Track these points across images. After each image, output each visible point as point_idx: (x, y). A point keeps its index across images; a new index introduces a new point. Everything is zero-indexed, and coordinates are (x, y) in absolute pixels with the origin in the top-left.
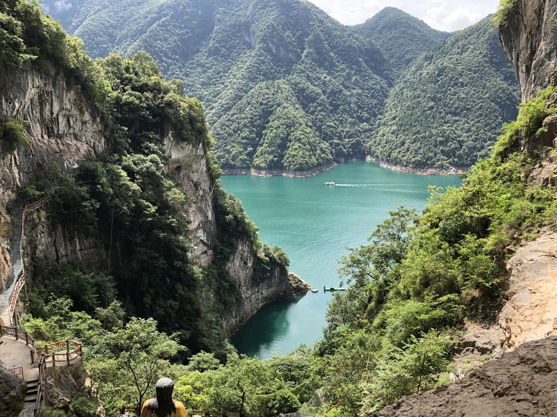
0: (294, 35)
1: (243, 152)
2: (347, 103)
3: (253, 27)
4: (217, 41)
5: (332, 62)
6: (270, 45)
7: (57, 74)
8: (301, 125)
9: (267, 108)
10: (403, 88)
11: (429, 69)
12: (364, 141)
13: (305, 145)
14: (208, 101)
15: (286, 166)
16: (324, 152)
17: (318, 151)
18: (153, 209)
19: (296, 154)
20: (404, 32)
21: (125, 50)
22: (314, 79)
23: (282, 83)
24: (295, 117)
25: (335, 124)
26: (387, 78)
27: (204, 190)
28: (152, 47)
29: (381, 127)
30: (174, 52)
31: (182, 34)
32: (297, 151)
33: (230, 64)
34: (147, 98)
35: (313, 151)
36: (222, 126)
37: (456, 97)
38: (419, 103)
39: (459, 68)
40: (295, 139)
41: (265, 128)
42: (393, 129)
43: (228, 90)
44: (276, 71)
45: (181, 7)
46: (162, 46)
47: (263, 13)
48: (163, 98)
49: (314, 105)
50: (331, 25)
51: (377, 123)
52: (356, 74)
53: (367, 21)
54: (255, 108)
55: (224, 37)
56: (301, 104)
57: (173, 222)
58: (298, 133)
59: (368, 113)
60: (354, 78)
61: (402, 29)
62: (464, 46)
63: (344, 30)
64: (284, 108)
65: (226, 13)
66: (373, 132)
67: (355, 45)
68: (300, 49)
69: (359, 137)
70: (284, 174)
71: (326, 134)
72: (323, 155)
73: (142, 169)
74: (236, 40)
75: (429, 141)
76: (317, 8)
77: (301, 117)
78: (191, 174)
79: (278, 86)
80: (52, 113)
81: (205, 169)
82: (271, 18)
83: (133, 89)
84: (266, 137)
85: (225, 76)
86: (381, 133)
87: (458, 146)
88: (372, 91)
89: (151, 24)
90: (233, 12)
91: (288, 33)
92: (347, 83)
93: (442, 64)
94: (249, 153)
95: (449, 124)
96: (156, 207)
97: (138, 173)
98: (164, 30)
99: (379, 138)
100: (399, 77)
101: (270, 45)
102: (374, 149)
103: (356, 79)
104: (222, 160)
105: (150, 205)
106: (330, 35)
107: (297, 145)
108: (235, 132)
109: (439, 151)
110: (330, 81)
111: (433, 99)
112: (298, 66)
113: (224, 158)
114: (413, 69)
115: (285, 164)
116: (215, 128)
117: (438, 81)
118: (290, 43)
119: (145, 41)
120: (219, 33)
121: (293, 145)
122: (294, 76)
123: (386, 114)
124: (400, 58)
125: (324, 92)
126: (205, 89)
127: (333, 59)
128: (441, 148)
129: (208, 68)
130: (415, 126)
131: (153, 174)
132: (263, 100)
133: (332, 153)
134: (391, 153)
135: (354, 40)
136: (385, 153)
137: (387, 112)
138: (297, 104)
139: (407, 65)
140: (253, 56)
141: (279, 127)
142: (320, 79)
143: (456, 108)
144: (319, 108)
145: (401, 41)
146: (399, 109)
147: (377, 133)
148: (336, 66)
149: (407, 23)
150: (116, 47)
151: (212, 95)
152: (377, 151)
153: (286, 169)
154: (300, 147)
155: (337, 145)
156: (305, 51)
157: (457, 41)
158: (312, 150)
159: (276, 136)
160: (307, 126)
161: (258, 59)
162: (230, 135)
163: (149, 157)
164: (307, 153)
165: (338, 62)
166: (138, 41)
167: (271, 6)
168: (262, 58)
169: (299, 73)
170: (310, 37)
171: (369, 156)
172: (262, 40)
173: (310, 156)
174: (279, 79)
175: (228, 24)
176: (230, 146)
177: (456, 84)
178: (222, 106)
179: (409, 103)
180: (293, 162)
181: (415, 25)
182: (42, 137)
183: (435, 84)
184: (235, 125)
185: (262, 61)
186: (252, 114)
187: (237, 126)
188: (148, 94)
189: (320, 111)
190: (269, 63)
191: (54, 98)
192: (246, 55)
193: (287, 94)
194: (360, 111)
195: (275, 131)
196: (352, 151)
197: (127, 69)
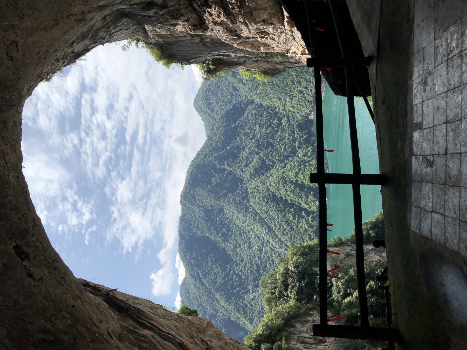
0: (215, 176)
1: (305, 219)
3: (208, 207)
4: (217, 234)
5: (234, 148)
6: (221, 194)
7: (287, 331)
8: (284, 172)
9: (271, 198)
10: (256, 93)
12: (297, 121)
14: (262, 244)
16: (306, 154)
18: (372, 283)
20: (213, 93)
21: (222, 307)
23: (251, 185)
24: (278, 176)
25: (283, 145)
26: (247, 105)
27: (351, 250)
28: (221, 286)
30: (225, 268)
31: (212, 261)
33: (234, 226)
34: (292, 282)
35: (306, 163)
36: (284, 234)
41: (286, 201)
42: (289, 100)
43: (254, 228)
44: (241, 190)
45: (192, 260)
46: (220, 277)
47: (198, 198)
48: (292, 272)
49: (267, 161)
51: (282, 112)
52: (244, 129)
53: (203, 120)
54: (270, 207)
55: (214, 229)
56: (267, 171)
57: (380, 271)
58: (291, 175)
59: (274, 119)
60: (247, 130)
61: (211, 94)
63: (211, 139)
64: (270, 185)
65: (197, 227)
66: (290, 114)
67: (223, 131)
68: (224, 171)
69: (293, 126)
71: (291, 152)
72: (309, 155)
73: (343, 288)
74: (217, 220)
75: (300, 72)
76: (195, 158)
78: (340, 258)
80: (310, 338)
81: (335, 248)
82: (202, 193)
83: (286, 290)
84: (294, 200)
85: (243, 229)
86: (291, 109)
88: (257, 116)
89: (203, 285)
90: (196, 221)
91: (213, 180)
94: (306, 214)
96: (371, 281)
97: (346, 291)
98: (209, 275)
99: (295, 110)
100: (246, 96)
101: (221, 194)
103: (248, 129)
104: (313, 237)
105: (369, 284)
106: (214, 149)
107: (300, 175)
108: (289, 224)
110: (249, 149)
112: (238, 173)
113: (310, 235)
114: (241, 85)
116: (286, 240)
118: (221, 179)
119: (217, 290)
120: (211, 233)
121: (301, 178)
122: (245, 177)
123: (276, 104)
124: (232, 95)
125: (258, 153)
126: (253, 247)
127: (232, 147)
129: (237, 243)
130: (287, 83)
131: (346, 281)
132: (264, 201)
133: (307, 147)
134: (308, 101)
135: (219, 131)
137: (274, 105)
138: (267, 174)
139: (237, 90)
140: (229, 207)
141: (286, 189)
142: (247, 157)
144: (270, 157)
145: (219, 95)
146: (273, 96)
147: (291, 111)
148: (238, 144)
149: (206, 91)
150: (219, 313)
151: (258, 241)
152: (306, 111)
154: (302, 173)
155: (300, 143)
156: (226, 168)
159: (293, 193)
160: (284, 167)
161: (232, 204)
162: (291, 228)
163: (334, 283)
164: (308, 167)
165: (235, 143)
166: (216, 296)
167: (194, 192)
168: (231, 200)
170: (216, 164)
171: (310, 117)
172: (218, 200)
173: (309, 165)
174: (247, 189)
175: (205, 225)
176: (301, 229)
178: (267, 233)
179: (269, 89)
181: (207, 85)
182: (326, 345)
184: (284, 224)
185: (233, 200)
186: (275, 210)
187: (284, 223)
188: (290, 281)
189: (272, 157)
190: (235, 195)
191: (301, 336)
192: (228, 212)
194: (273, 125)
195: (289, 193)
196: (305, 130)
197: (273, 293)
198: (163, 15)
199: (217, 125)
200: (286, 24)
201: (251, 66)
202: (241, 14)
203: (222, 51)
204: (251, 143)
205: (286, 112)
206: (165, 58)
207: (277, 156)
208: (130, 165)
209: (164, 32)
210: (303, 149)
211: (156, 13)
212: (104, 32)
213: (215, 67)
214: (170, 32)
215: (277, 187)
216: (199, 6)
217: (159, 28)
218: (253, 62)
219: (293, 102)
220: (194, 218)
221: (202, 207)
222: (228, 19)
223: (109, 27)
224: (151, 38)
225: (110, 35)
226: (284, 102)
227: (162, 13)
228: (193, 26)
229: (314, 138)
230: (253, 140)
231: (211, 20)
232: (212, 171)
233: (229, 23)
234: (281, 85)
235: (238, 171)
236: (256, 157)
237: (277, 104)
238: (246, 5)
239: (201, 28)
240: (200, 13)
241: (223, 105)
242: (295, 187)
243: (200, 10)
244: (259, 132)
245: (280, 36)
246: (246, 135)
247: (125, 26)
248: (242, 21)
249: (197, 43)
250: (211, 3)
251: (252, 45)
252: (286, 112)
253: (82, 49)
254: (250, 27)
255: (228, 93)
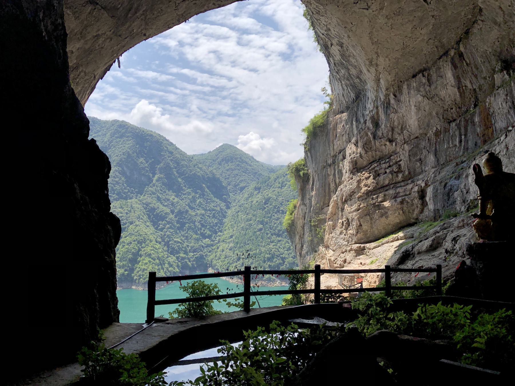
0: (147, 162)
2: (192, 222)
5: (179, 186)
6: (125, 169)
8: (151, 241)
10: (238, 212)
11: (258, 198)
13: (154, 260)
15: (136, 279)
17: (167, 265)
19: (146, 268)
20: (238, 165)
22: (164, 200)
24: (146, 234)
25: (181, 240)
26: (225, 201)
29: (221, 243)
32: (147, 265)
35: (161, 265)
37: (278, 221)
38: (251, 225)
39: (280, 199)
40: (145, 254)
42: (230, 246)
44: (129, 191)
47: (120, 141)
49: (163, 222)
50: (179, 156)
51: (217, 239)
52: (199, 197)
56: (151, 222)
58: (148, 249)
59: (210, 231)
60: (198, 201)
61: (237, 163)
62: (283, 182)
63: (190, 160)
64: (137, 226)
66: (214, 247)
67: (199, 174)
68: (152, 173)
70: (133, 287)
71: (173, 248)
72: (170, 269)
76: (168, 141)
77: (152, 234)
79: (131, 206)
82: (127, 146)
86: (221, 248)
87: (282, 262)
88: (214, 212)
91: (142, 160)
92: (192, 205)
93: (267, 195)
95: (274, 244)
100: (235, 200)
101: (125, 169)
102: (215, 262)
103: (200, 202)
106: (178, 164)
107: (147, 259)
109: (267, 266)
110: (178, 202)
111: (262, 223)
112: (150, 189)
114: (246, 196)
115: (135, 278)
117: (265, 208)
118: (143, 169)
122: (146, 197)
123: (225, 232)
124: (235, 186)
125: (172, 212)
128: (269, 263)
130: (248, 244)
133: (178, 266)
134: (229, 267)
135: (199, 170)
136: (224, 267)
137: (225, 230)
141: (131, 243)
142: (168, 200)
143: (279, 231)
144: (168, 226)
145: (236, 172)
146: (235, 229)
147: (218, 248)
148: (183, 190)
149: (241, 158)
152: (218, 264)
153: (135, 282)
154: (150, 262)
155: (183, 258)
156: (156, 176)
157: (278, 177)
158: (161, 264)
160: (157, 242)
164: (157, 267)
165: (185, 186)
167: (128, 137)
169: (150, 194)
170: (162, 165)
172: (117, 163)
173: (159, 269)
174: (131, 198)
177: (278, 211)
179: (243, 225)
180: (143, 275)
181: (247, 160)
183: (263, 210)
185: (117, 182)
189: (169, 228)
190: (123, 184)
193: (139, 213)
194: (203, 229)
195: (127, 247)
196: (196, 264)
198: (367, 135)
199: (204, 168)
200: (358, 245)
201: (300, 210)
202: (367, 206)
203: (318, 183)
204: (184, 205)
205: (217, 243)
206: (314, 128)
207: (169, 233)
208: (154, 71)
209: (339, 130)
210: (177, 261)
211: (368, 129)
212: (344, 75)
213: (300, 174)
214: (339, 137)
215: (133, 233)
216: (374, 168)
217: (343, 126)
218: (304, 212)
219: (228, 250)
220: (96, 135)
221: (109, 145)
222: (363, 193)
223: (348, 80)
224: (333, 117)
225: (339, 79)
226: (228, 241)
227: (369, 134)
228: (356, 161)
229: (188, 273)
230: (187, 208)
231: (362, 178)
232: (153, 160)
233: (359, 194)
234: (246, 237)
235: (153, 189)
236: (168, 211)
237: (227, 233)
238: (376, 210)
239: (354, 169)
240: (367, 168)
241: (226, 176)
242: (133, 254)
243: (370, 169)
244: (197, 214)
245: (344, 240)
246: (194, 200)
247: (347, 94)
248: (361, 206)
249: (326, 161)
250: (378, 179)
251: (334, 214)
252: (217, 243)
253: (331, 53)
254: (355, 213)
255: (238, 181)
